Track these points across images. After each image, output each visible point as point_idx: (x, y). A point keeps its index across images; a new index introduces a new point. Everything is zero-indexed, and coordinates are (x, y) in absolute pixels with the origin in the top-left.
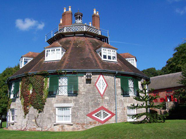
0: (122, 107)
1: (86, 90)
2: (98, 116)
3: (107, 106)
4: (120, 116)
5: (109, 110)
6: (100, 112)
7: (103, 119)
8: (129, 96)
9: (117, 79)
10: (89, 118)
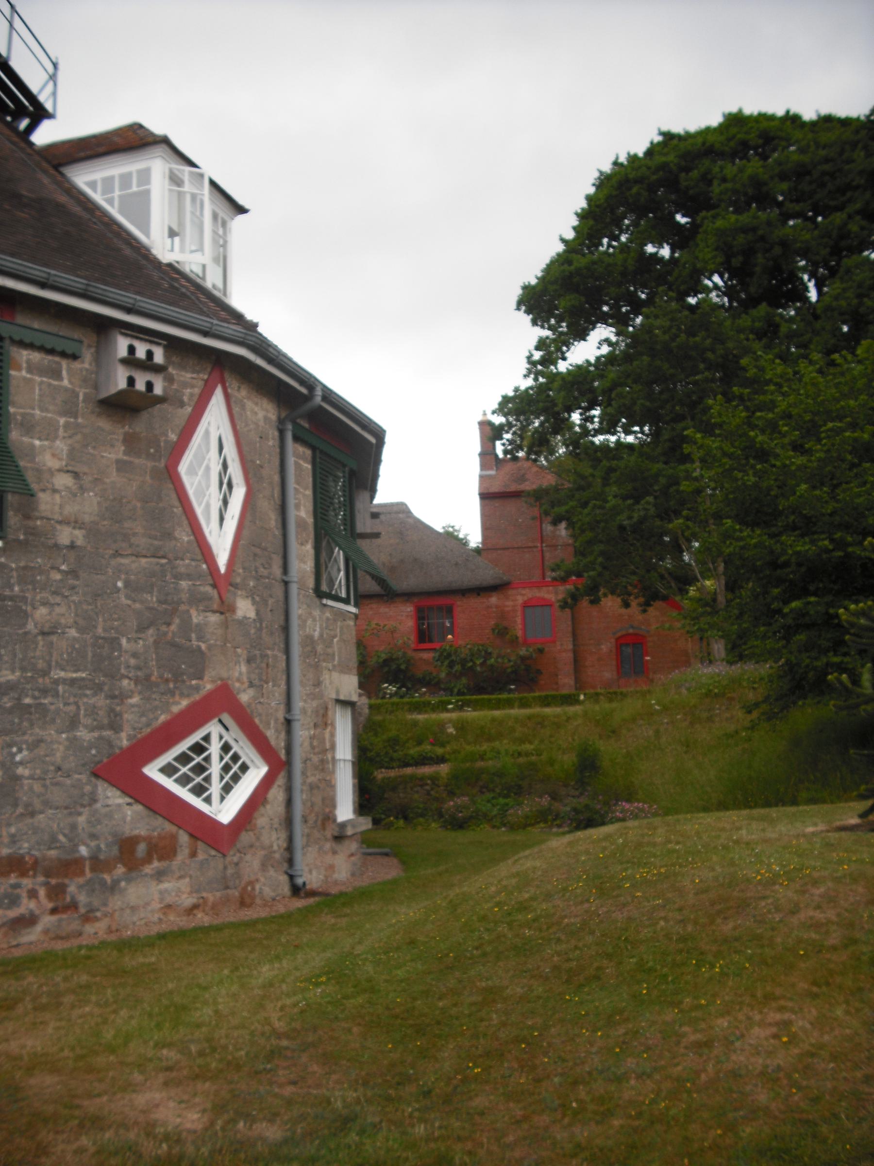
2: (183, 781)
5: (257, 721)
6: (196, 737)
10: (112, 797)
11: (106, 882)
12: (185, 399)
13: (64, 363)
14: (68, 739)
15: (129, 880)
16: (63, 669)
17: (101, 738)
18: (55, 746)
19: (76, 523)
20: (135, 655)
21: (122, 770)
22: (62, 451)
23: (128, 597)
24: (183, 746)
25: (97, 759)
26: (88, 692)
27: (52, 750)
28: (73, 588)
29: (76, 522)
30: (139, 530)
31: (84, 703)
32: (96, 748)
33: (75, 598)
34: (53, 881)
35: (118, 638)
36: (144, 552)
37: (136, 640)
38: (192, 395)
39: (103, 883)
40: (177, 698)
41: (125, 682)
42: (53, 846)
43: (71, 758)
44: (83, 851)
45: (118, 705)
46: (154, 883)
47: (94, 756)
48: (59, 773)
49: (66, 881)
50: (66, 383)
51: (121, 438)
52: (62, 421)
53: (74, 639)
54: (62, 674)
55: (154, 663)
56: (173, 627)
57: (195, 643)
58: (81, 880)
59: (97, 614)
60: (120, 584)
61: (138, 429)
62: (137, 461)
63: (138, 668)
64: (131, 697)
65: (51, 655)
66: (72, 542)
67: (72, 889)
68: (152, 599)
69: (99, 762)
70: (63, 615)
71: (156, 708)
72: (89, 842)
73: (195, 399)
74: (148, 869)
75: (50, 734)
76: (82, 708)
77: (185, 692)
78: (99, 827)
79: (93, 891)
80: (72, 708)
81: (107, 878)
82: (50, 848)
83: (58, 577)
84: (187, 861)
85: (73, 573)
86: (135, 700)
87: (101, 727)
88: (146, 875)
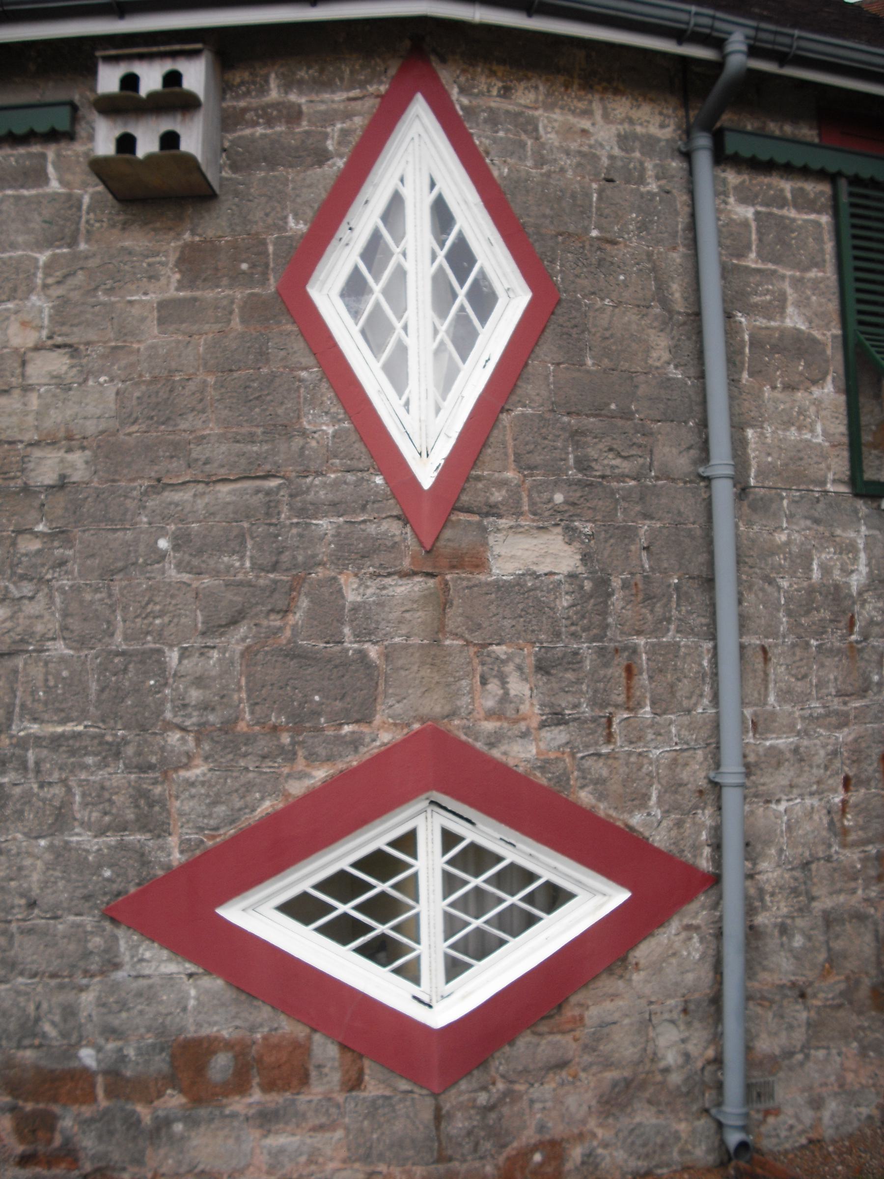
0: (841, 735)
1: (97, 404)
2: (342, 931)
3: (532, 710)
4: (801, 894)
5: (585, 797)
6: (376, 837)
7: (442, 1000)
8: (25, 483)
9: (731, 203)
10: (158, 963)
11: (139, 1121)
12: (330, 145)
13: (51, 152)
14: (51, 848)
15: (192, 1122)
16: (35, 720)
17: (122, 846)
18: (28, 862)
19: (70, 440)
20: (199, 682)
21: (180, 907)
22: (41, 311)
23: (179, 567)
24: (342, 857)
25: (115, 887)
26: (90, 760)
27: (20, 869)
28: (62, 563)
29: (69, 438)
30: (213, 429)
31: (80, 783)
32: (111, 866)
33: (66, 583)
34: (29, 1107)
35: (160, 652)
36: (223, 472)
37: (203, 651)
38: (344, 133)
39: (133, 1122)
40: (300, 764)
41: (174, 738)
42: (26, 1042)
43: (61, 884)
44: (87, 1056)
45: (155, 782)
46: (257, 1133)
47: (110, 880)
48: (36, 911)
49: (56, 1109)
50: (55, 185)
51: (173, 258)
52: (43, 258)
53: (63, 659)
54: (35, 728)
55: (244, 695)
56: (296, 618)
57: (351, 645)
58: (87, 1111)
59: (112, 608)
60: (163, 544)
61: (210, 233)
62: (209, 294)
63: (206, 707)
64: (187, 766)
65: (13, 692)
66: (63, 477)
67: (67, 1123)
68: (242, 565)
69: (119, 894)
70: (40, 617)
71: (249, 787)
72: (101, 1041)
73: (354, 139)
74: (238, 1105)
75: (14, 839)
76: (77, 791)
77: (322, 751)
78: (124, 1015)
79: (111, 1133)
80: (58, 791)
81: (143, 1112)
82: (19, 1046)
83: (35, 545)
84: (340, 1098)
85: (60, 534)
86: (198, 771)
87: (123, 827)
88: (234, 1116)
